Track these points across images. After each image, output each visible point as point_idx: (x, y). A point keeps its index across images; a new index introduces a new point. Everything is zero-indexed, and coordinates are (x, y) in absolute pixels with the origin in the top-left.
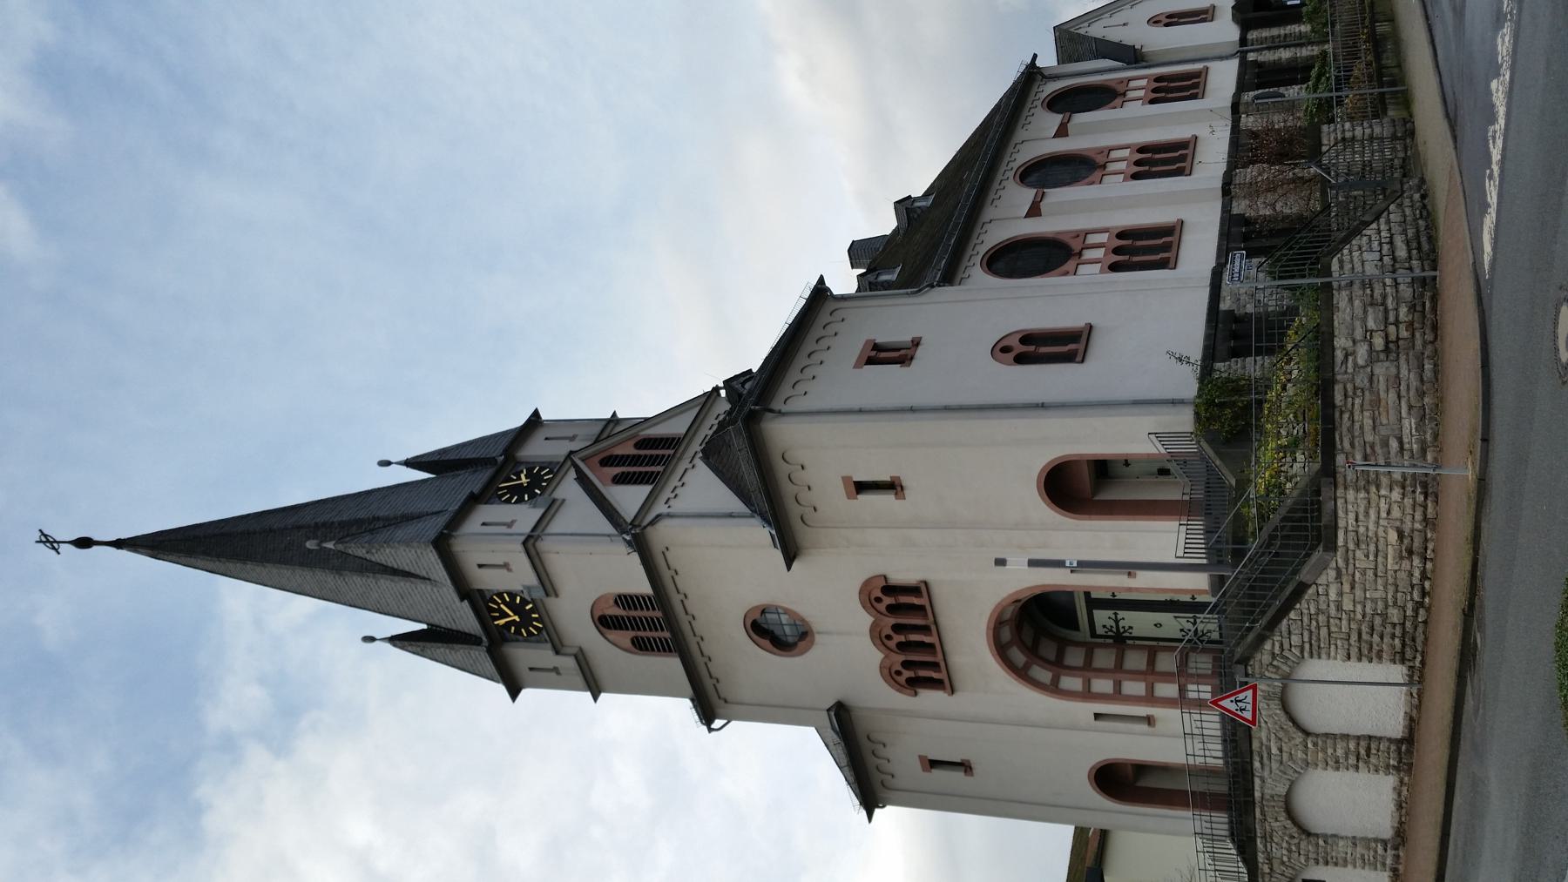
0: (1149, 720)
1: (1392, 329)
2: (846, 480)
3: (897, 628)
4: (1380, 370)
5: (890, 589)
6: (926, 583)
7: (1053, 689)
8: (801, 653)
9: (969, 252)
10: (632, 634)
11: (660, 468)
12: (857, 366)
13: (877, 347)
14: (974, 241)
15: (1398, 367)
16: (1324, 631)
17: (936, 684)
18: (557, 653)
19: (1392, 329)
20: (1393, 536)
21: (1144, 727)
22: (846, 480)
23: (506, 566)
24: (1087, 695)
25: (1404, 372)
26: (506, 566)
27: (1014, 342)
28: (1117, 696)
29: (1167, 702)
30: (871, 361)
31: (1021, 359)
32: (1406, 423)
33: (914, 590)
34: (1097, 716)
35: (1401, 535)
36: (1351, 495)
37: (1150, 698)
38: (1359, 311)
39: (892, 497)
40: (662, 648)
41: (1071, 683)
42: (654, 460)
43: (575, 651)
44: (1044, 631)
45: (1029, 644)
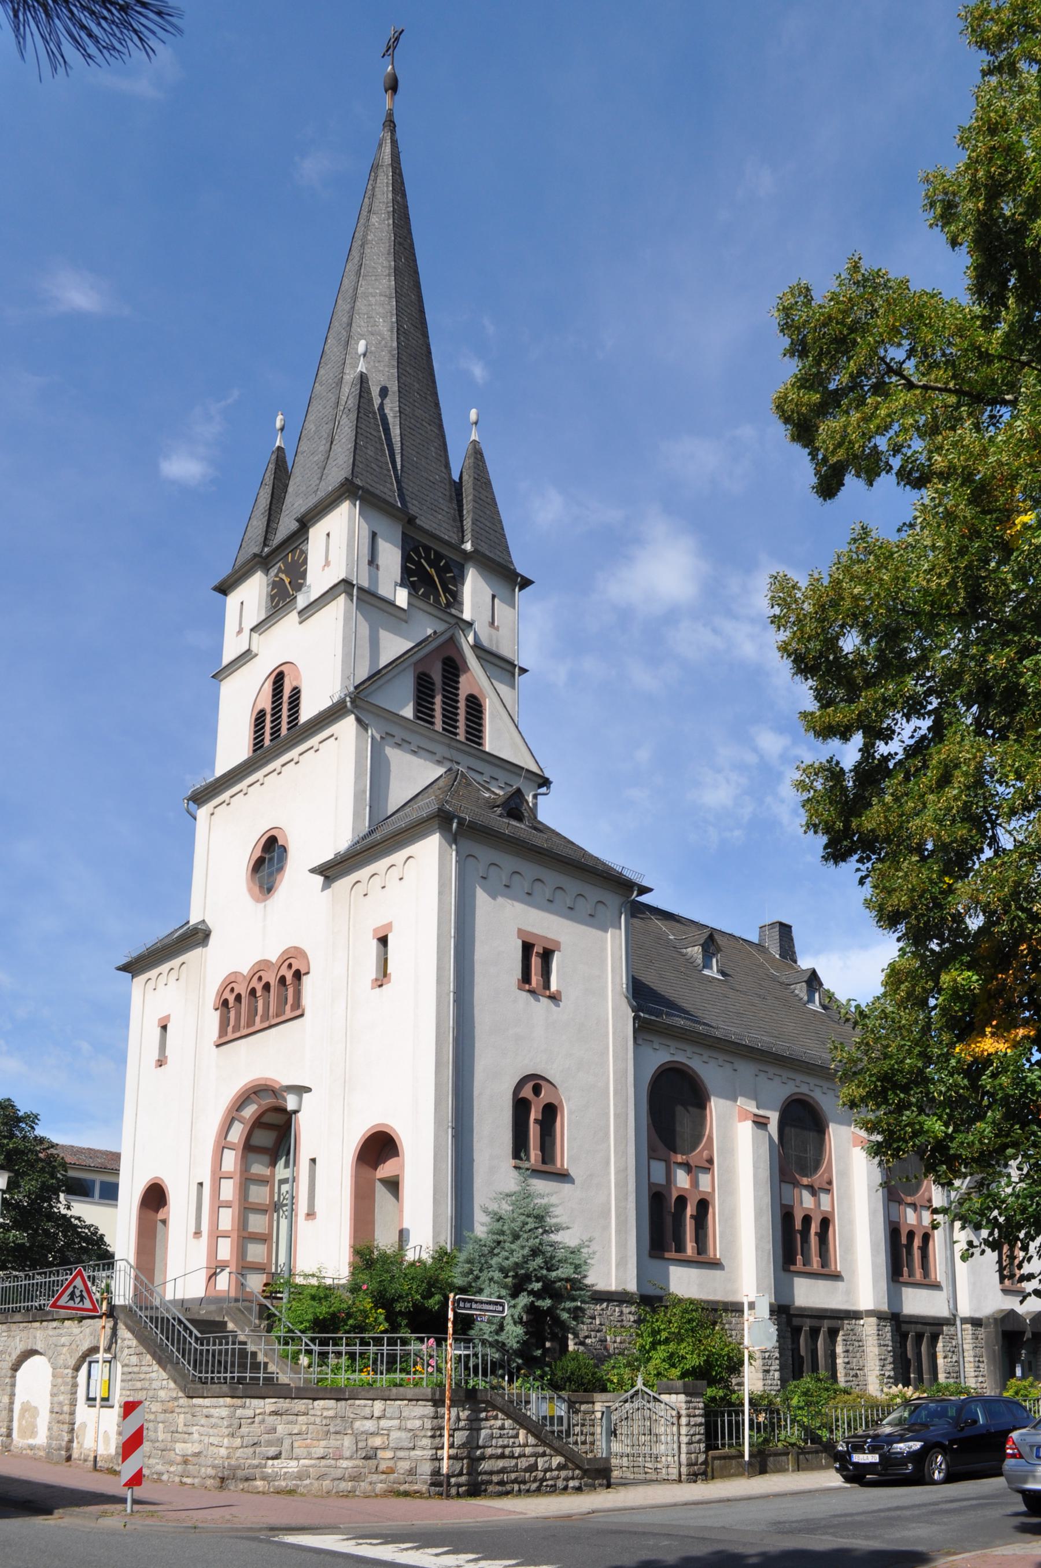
0: (198, 1233)
1: (389, 1454)
2: (389, 926)
3: (267, 987)
4: (348, 1442)
5: (298, 975)
6: (302, 1015)
7: (222, 1146)
8: (250, 890)
9: (689, 1049)
10: (269, 711)
11: (439, 726)
12: (520, 930)
13: (547, 956)
14: (706, 1054)
15: (351, 1458)
16: (139, 1385)
17: (223, 1031)
18: (252, 630)
19: (389, 1454)
20: (196, 1448)
21: (192, 1229)
22: (389, 926)
23: (327, 563)
24: (218, 1176)
25: (344, 1464)
26: (327, 563)
27: (545, 1096)
28: (219, 1204)
29: (213, 1250)
30: (527, 948)
31: (521, 1107)
32: (294, 1463)
33: (297, 1003)
34: (201, 1184)
35: (197, 1455)
36: (224, 1412)
37: (216, 1235)
38: (410, 1424)
39: (374, 976)
40: (258, 744)
41: (230, 1160)
42: (450, 718)
43: (254, 649)
44: (268, 1128)
45: (264, 1120)
